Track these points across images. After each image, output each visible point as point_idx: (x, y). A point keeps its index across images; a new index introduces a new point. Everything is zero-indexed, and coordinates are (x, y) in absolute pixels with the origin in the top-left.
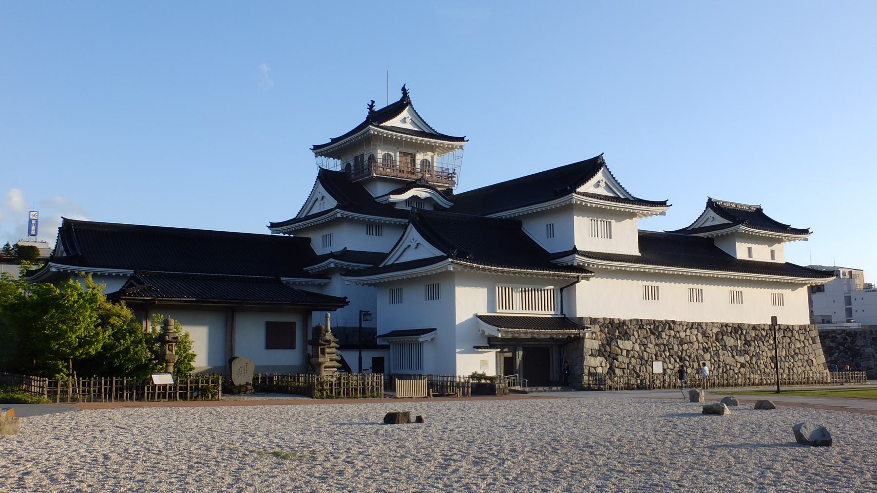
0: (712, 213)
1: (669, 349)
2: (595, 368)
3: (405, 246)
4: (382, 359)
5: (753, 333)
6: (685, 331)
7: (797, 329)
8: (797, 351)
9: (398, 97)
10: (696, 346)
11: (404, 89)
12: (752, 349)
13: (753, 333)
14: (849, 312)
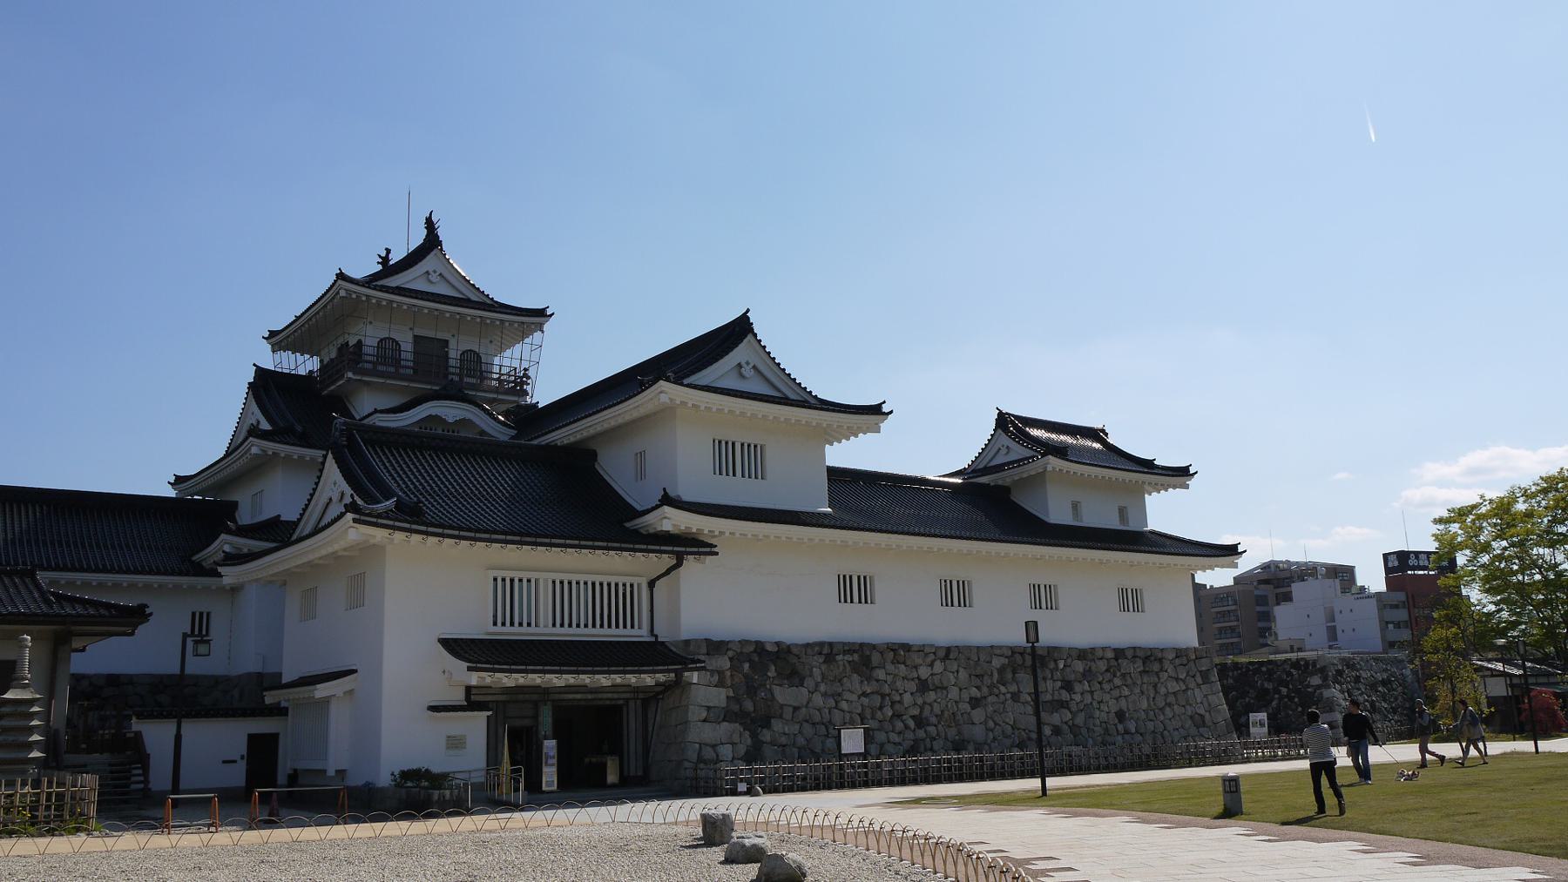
0: (1004, 440)
1: (893, 703)
2: (714, 746)
3: (324, 500)
4: (274, 738)
5: (1079, 666)
6: (931, 665)
7: (1171, 656)
8: (1171, 699)
9: (419, 237)
10: (954, 693)
11: (430, 224)
12: (1078, 698)
13: (1079, 666)
14: (1332, 633)
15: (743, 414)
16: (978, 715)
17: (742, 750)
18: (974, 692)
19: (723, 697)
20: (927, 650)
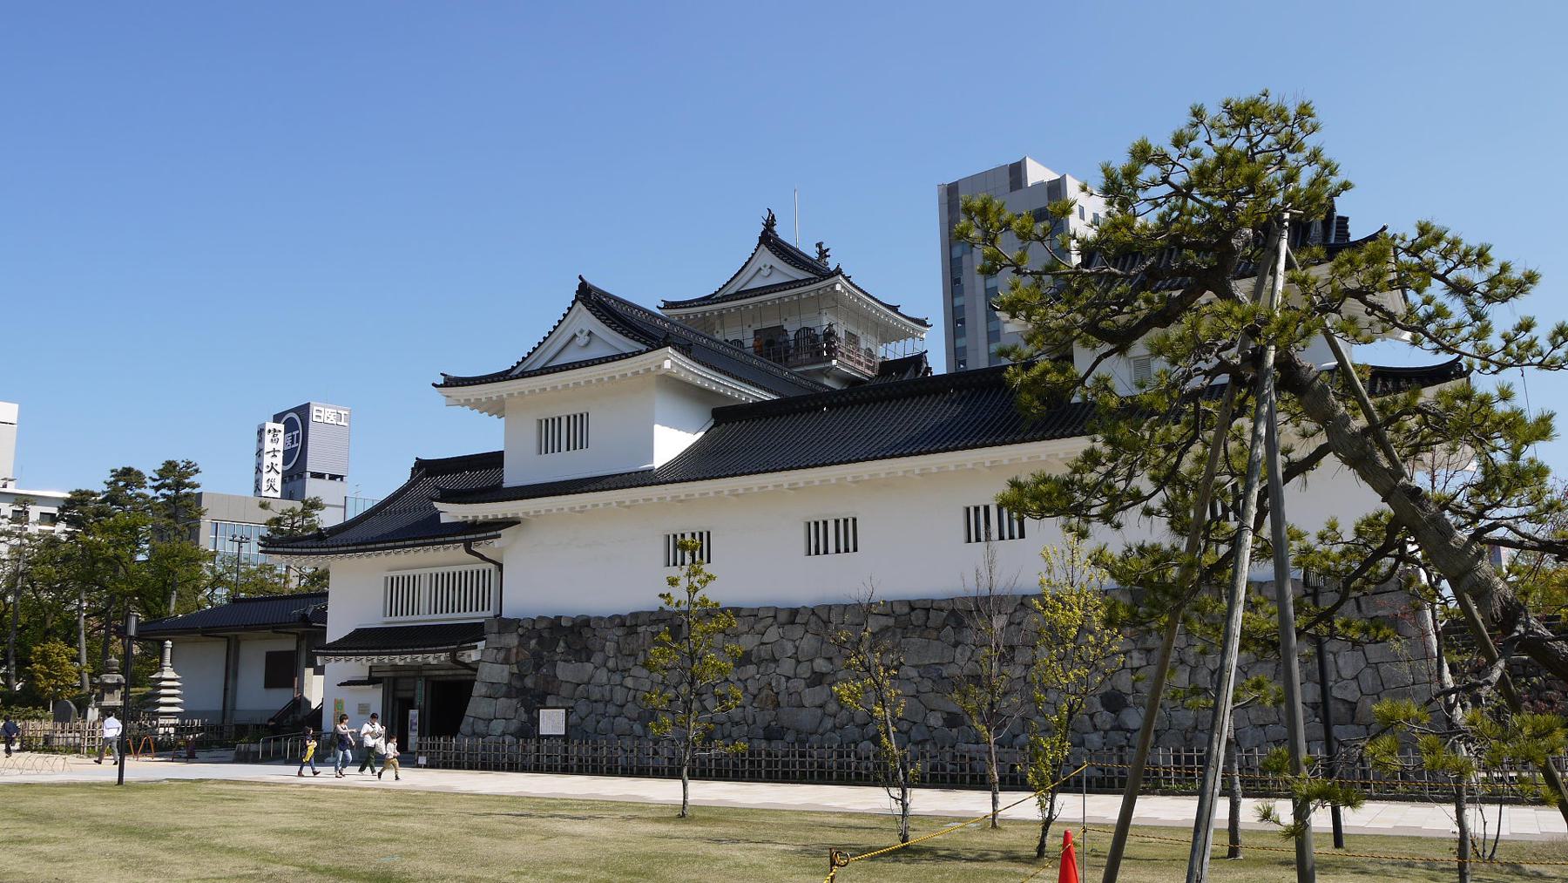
15: (555, 388)
16: (812, 696)
17: (514, 725)
18: (821, 665)
19: (506, 673)
20: (761, 614)
